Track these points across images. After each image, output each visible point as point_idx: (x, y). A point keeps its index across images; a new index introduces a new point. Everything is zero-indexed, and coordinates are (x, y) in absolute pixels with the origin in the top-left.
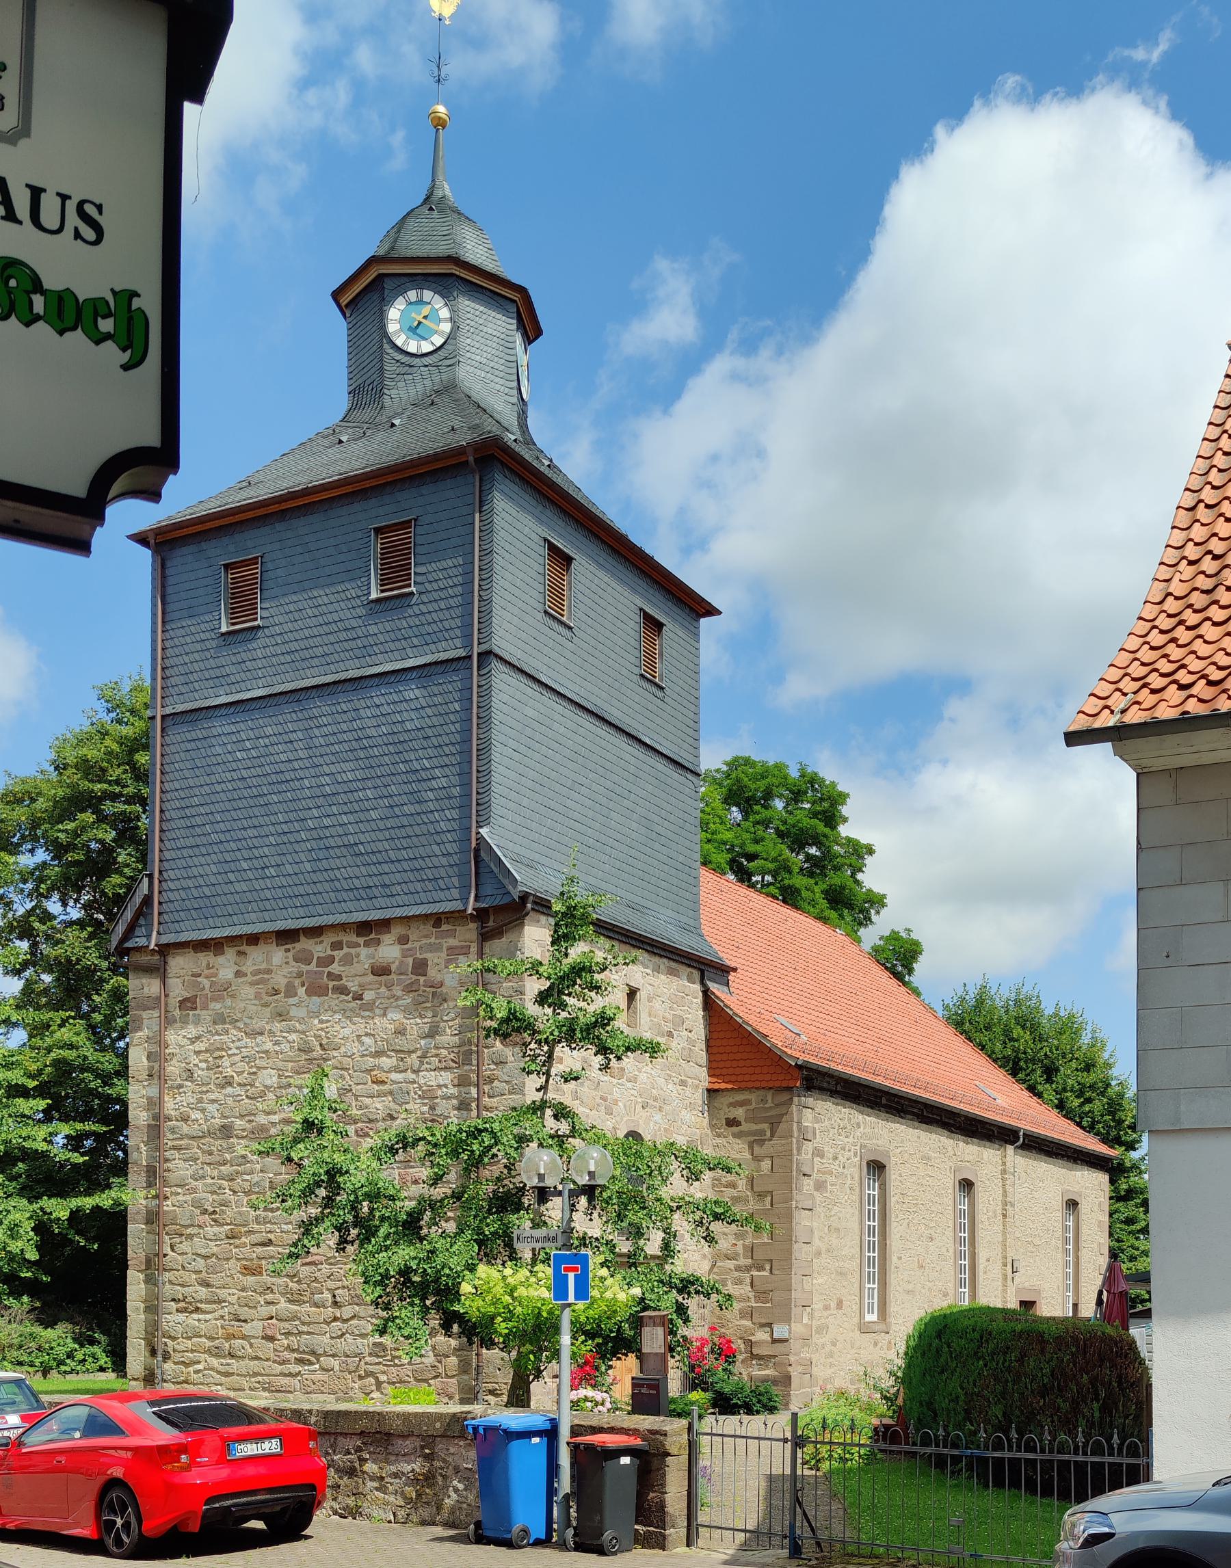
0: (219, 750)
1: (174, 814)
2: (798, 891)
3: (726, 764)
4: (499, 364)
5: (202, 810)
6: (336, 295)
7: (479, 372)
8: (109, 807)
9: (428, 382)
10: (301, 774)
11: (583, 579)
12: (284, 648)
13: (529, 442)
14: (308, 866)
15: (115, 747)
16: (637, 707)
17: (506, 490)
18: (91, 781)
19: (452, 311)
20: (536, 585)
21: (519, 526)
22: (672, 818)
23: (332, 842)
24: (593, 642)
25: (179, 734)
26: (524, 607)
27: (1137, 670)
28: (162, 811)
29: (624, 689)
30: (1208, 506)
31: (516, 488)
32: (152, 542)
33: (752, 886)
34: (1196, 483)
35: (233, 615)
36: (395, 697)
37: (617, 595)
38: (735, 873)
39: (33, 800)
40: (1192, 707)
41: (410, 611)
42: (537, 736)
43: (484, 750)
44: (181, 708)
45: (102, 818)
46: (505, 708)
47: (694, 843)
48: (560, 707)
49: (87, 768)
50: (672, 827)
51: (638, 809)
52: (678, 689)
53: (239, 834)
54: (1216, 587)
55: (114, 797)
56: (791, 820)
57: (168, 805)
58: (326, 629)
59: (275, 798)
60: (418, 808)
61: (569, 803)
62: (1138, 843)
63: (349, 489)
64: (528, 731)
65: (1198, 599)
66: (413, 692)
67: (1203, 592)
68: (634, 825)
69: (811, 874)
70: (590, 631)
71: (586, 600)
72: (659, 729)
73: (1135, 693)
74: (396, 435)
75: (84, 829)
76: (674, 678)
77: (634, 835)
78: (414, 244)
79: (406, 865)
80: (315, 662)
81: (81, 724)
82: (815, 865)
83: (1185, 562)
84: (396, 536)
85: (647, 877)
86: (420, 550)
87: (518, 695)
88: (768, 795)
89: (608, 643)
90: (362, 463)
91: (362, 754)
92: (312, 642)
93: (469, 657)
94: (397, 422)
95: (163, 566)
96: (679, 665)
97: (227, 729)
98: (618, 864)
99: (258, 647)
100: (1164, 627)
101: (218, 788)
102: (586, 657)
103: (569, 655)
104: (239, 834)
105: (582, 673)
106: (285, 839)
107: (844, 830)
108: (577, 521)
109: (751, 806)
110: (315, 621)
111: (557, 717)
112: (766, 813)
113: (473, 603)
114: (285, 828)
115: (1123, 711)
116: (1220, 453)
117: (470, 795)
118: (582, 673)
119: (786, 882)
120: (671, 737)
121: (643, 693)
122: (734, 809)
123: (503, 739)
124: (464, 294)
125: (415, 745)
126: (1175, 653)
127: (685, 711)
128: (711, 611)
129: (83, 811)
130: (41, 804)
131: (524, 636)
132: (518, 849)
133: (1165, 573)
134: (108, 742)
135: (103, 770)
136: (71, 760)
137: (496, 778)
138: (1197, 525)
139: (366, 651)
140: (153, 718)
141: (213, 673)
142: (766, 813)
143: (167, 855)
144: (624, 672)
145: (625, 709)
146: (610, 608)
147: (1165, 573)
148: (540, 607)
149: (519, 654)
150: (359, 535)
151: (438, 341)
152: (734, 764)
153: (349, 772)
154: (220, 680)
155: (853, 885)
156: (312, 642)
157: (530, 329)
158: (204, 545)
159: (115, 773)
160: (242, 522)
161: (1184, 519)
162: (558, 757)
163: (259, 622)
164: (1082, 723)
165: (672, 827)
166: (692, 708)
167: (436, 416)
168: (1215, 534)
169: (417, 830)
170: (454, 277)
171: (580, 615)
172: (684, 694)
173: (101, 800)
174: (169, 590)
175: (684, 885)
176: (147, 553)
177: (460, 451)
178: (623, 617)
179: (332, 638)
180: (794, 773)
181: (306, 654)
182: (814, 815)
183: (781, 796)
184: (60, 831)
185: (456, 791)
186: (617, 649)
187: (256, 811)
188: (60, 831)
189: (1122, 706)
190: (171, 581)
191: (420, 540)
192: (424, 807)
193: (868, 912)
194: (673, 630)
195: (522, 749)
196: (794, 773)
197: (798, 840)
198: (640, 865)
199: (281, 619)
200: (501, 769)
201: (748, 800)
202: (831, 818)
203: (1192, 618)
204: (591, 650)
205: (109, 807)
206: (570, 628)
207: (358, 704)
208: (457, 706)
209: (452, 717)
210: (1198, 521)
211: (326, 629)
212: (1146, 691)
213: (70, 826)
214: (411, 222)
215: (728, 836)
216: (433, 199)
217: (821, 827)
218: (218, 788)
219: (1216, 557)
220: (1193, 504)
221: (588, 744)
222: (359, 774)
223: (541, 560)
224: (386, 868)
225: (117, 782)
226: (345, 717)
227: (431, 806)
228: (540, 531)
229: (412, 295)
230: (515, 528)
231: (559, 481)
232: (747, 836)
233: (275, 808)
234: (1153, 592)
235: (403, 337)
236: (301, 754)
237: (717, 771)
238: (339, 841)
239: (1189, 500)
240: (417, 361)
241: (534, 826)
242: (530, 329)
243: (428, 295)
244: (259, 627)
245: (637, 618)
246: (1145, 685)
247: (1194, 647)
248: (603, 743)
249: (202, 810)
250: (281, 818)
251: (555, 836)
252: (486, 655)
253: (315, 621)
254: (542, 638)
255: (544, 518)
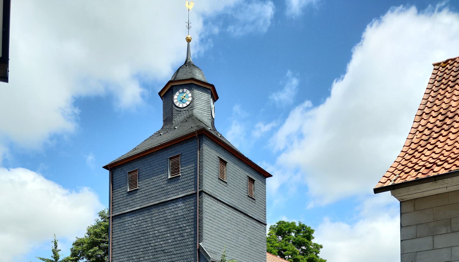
0: (127, 225)
1: (115, 244)
2: (299, 260)
3: (277, 223)
4: (206, 108)
5: (123, 242)
6: (160, 94)
7: (200, 111)
8: (102, 245)
9: (185, 115)
10: (149, 230)
11: (230, 168)
12: (144, 195)
13: (215, 130)
14: (151, 257)
15: (104, 228)
16: (247, 205)
17: (207, 143)
18: (98, 238)
19: (192, 94)
20: (216, 171)
21: (211, 154)
22: (258, 238)
23: (158, 250)
24: (233, 187)
25: (117, 221)
26: (212, 177)
27: (400, 167)
28: (112, 243)
29: (243, 200)
30: (426, 114)
31: (210, 143)
32: (109, 168)
33: (285, 259)
34: (422, 107)
35: (131, 186)
36: (176, 206)
37: (240, 172)
38: (280, 256)
39: (83, 244)
40: (420, 176)
41: (179, 181)
42: (217, 215)
43: (201, 220)
44: (117, 214)
45: (100, 248)
46: (207, 207)
47: (264, 246)
48: (224, 207)
49: (96, 235)
50: (258, 241)
51: (247, 236)
52: (259, 199)
53: (133, 249)
54: (429, 138)
55: (104, 242)
56: (296, 239)
57: (114, 242)
58: (156, 188)
59: (142, 238)
60: (182, 238)
61: (226, 235)
62: (401, 225)
63: (162, 147)
64: (214, 214)
65: (423, 143)
66: (180, 204)
67: (425, 140)
68: (246, 241)
69: (303, 255)
70: (232, 183)
71: (231, 174)
72: (253, 212)
73: (399, 174)
74: (176, 131)
75: (95, 251)
76: (258, 196)
77: (246, 243)
78: (181, 76)
79: (179, 255)
80: (153, 198)
81: (93, 223)
82: (304, 252)
83: (418, 132)
84: (175, 160)
85: (250, 256)
86: (182, 163)
87: (211, 203)
88: (290, 232)
89: (238, 187)
90: (166, 140)
91: (166, 224)
92: (152, 192)
93: (196, 193)
94: (176, 127)
95: (112, 175)
96: (260, 192)
97: (129, 219)
98: (241, 252)
99: (138, 195)
100: (410, 153)
101: (127, 236)
102: (231, 191)
103: (226, 191)
104: (133, 249)
105: (230, 196)
106: (145, 249)
107: (313, 241)
108: (228, 151)
109: (284, 235)
110: (153, 186)
111: (222, 209)
112: (289, 237)
113: (197, 178)
114: (145, 246)
115: (395, 180)
116: (431, 97)
117: (197, 234)
118: (230, 196)
119: (295, 257)
120: (257, 214)
121: (249, 201)
122: (280, 237)
123: (206, 216)
124: (195, 88)
125: (181, 220)
126: (414, 161)
127: (262, 206)
128: (270, 176)
129: (96, 246)
130: (84, 246)
131: (212, 186)
132: (211, 249)
133: (411, 136)
134: (102, 227)
135: (101, 235)
136: (92, 232)
137: (204, 228)
138: (423, 120)
139: (167, 194)
140: (110, 217)
141: (125, 203)
142: (289, 237)
143: (114, 256)
144: (243, 195)
145: (243, 206)
146: (238, 176)
147: (411, 136)
148: (217, 177)
149: (211, 191)
150: (165, 160)
151: (188, 103)
152: (279, 223)
153: (163, 229)
154: (127, 205)
155: (316, 257)
156: (152, 192)
157: (215, 97)
158: (123, 168)
159: (104, 235)
160: (133, 160)
161: (418, 119)
162: (223, 221)
163: (138, 188)
164: (380, 185)
165: (258, 241)
166: (264, 205)
167: (187, 124)
168: (429, 122)
169: (182, 245)
170: (193, 84)
171: (229, 179)
172: (261, 201)
173: (100, 243)
174: (114, 181)
175: (261, 258)
176: (108, 172)
177: (193, 133)
178: (242, 179)
179: (158, 191)
180: (297, 225)
181: (151, 196)
182: (304, 237)
183: (293, 232)
184: (90, 252)
185: (193, 233)
186: (241, 188)
187: (137, 242)
188: (90, 252)
189: (394, 179)
190: (114, 178)
191: (182, 160)
192: (184, 238)
193: (307, 252)
194: (258, 182)
195: (212, 219)
196: (297, 225)
197: (299, 244)
198: (248, 252)
199: (144, 186)
200: (206, 225)
201: (283, 234)
202: (309, 238)
203: (420, 149)
204: (233, 189)
205: (102, 245)
206: (226, 183)
207: (165, 209)
208: (193, 208)
209: (192, 211)
210: (423, 119)
211: (156, 188)
212: (403, 173)
213: (92, 250)
214: (181, 70)
215: (277, 244)
216: (187, 62)
217: (306, 240)
218: (127, 236)
219: (429, 129)
220: (420, 114)
221: (232, 217)
222: (165, 230)
223: (217, 163)
224: (173, 256)
225: (104, 238)
226: (161, 213)
227: (186, 237)
228: (217, 155)
229: (181, 91)
230: (210, 154)
231: (223, 140)
232: (283, 244)
233: (142, 241)
234: (407, 142)
235: (178, 103)
236: (150, 225)
237: (274, 226)
238: (160, 249)
239: (420, 113)
240: (182, 110)
241: (216, 242)
242: (215, 97)
243: (185, 90)
244: (138, 189)
245: (246, 179)
246: (403, 171)
247: (421, 158)
248: (237, 217)
249: (123, 242)
250: (144, 243)
251: (222, 244)
252: (201, 192)
253: (153, 186)
254: (218, 186)
255: (218, 151)
